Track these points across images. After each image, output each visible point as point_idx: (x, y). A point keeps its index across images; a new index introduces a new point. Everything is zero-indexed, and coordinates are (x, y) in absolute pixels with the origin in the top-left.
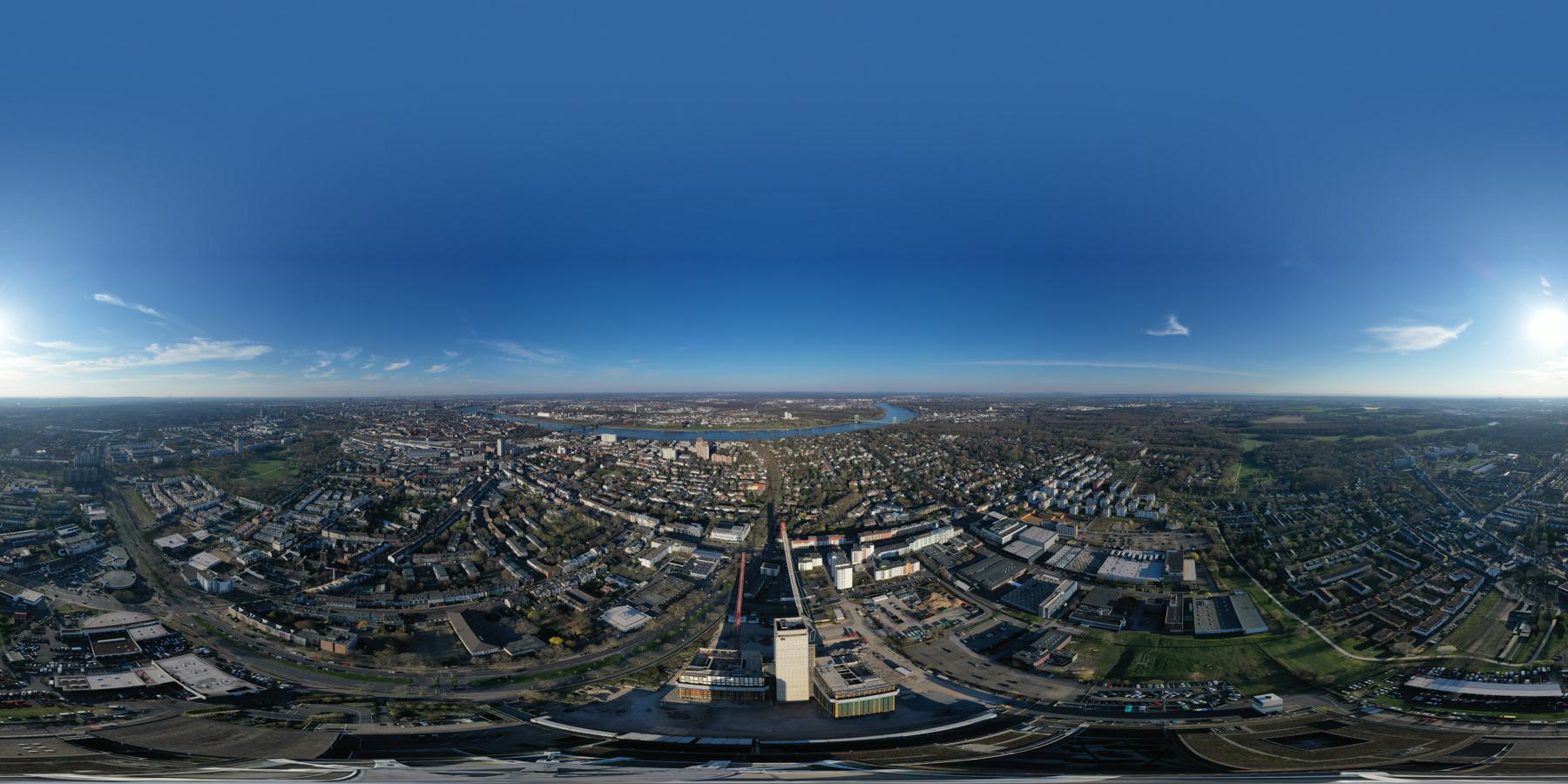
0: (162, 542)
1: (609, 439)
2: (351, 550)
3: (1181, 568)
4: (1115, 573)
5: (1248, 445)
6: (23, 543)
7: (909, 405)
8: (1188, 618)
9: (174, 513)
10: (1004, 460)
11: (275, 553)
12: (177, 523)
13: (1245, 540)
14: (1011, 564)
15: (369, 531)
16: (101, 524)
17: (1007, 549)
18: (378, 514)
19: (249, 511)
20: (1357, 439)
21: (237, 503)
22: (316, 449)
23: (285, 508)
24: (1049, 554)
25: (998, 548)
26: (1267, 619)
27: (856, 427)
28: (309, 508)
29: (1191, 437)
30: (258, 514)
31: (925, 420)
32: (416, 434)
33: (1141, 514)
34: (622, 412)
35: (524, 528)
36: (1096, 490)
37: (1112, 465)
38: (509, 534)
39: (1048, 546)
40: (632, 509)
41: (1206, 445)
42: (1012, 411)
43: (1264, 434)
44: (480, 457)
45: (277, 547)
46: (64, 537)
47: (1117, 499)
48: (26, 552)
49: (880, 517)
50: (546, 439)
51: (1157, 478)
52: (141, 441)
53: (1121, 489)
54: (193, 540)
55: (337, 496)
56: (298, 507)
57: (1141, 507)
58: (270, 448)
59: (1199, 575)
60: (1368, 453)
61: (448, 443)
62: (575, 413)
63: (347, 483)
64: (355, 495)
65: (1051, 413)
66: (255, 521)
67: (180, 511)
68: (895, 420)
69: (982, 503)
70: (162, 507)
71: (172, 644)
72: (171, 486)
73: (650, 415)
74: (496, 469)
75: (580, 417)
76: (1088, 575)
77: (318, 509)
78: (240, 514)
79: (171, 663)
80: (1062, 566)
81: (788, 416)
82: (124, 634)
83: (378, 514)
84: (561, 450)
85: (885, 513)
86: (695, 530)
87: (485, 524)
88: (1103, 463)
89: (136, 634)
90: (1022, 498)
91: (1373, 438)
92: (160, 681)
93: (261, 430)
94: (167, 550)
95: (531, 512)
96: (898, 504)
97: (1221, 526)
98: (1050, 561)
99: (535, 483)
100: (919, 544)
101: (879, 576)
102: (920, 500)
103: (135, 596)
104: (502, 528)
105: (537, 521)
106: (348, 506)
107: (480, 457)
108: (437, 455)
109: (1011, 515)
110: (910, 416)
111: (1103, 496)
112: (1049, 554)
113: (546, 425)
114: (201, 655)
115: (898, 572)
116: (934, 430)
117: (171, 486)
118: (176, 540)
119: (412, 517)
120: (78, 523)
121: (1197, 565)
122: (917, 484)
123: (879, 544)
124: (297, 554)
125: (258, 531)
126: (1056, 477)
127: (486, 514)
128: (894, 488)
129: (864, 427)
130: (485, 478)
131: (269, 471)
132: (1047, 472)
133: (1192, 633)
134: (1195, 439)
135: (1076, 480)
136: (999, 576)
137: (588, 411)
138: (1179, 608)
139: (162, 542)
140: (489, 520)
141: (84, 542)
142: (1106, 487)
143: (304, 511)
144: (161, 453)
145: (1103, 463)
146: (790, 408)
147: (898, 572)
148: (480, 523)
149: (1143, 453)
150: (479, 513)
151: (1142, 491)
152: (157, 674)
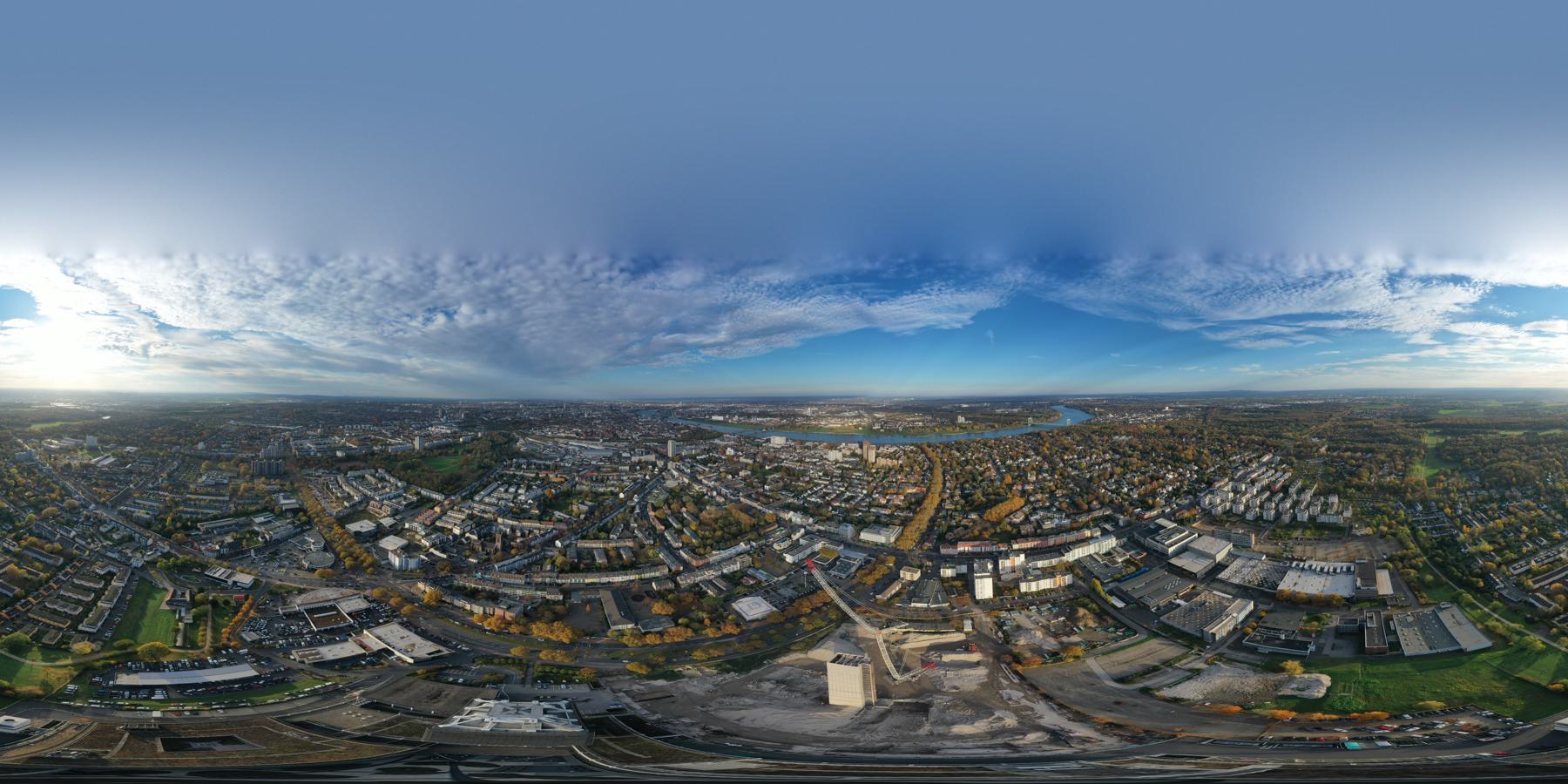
0: (354, 527)
1: (778, 441)
2: (523, 535)
3: (1374, 581)
4: (1297, 589)
5: (1430, 440)
6: (224, 531)
7: (1083, 405)
8: (1392, 638)
9: (360, 503)
10: (1176, 460)
11: (455, 536)
12: (364, 511)
13: (1442, 544)
14: (1177, 580)
15: (540, 519)
16: (295, 511)
17: (1174, 561)
18: (561, 500)
19: (430, 500)
20: (1541, 434)
21: (418, 494)
22: (493, 448)
23: (464, 499)
24: (1221, 567)
25: (1162, 557)
26: (1488, 632)
27: (1030, 430)
28: (487, 500)
29: (1372, 435)
30: (439, 503)
31: (1101, 420)
32: (590, 437)
33: (1323, 519)
34: (795, 415)
35: (682, 521)
36: (1273, 494)
37: (1291, 464)
38: (668, 526)
39: (1220, 557)
40: (788, 507)
41: (1388, 441)
42: (1189, 410)
43: (1445, 428)
44: (652, 458)
45: (457, 531)
46: (261, 524)
47: (1295, 504)
48: (229, 539)
49: (1039, 524)
50: (717, 441)
51: (1338, 480)
52: (322, 437)
53: (1301, 491)
54: (379, 525)
55: (512, 490)
56: (477, 498)
57: (1323, 512)
58: (448, 446)
59: (1395, 586)
60: (1553, 446)
61: (621, 445)
62: (749, 416)
63: (522, 478)
64: (529, 488)
65: (1228, 411)
66: (437, 509)
67: (366, 499)
68: (1069, 422)
69: (1151, 508)
70: (349, 497)
71: (368, 618)
72: (356, 478)
73: (823, 417)
74: (665, 469)
75: (753, 420)
76: (1264, 594)
77: (494, 501)
78: (424, 502)
79: (380, 631)
80: (1236, 581)
81: (961, 419)
82: (334, 608)
83: (547, 507)
84: (730, 452)
85: (1042, 520)
86: (848, 531)
87: (646, 517)
88: (1282, 462)
89: (346, 607)
90: (1195, 503)
91: (1558, 431)
92: (376, 648)
93: (440, 430)
94: (357, 534)
95: (692, 507)
96: (1059, 510)
97: (1413, 530)
98: (1222, 575)
99: (700, 482)
100: (1073, 556)
101: (1024, 587)
102: (1079, 503)
103: (338, 575)
104: (664, 522)
105: (696, 517)
106: (522, 498)
107: (652, 458)
108: (610, 454)
109: (1181, 522)
110: (1084, 417)
111: (1283, 500)
112: (1221, 567)
113: (720, 429)
114: (401, 624)
115: (1046, 584)
116: (1106, 431)
117: (356, 478)
118: (365, 526)
119: (579, 508)
120: (272, 511)
121: (1392, 575)
122: (1087, 487)
123: (1030, 554)
124: (475, 537)
125: (439, 518)
126: (1232, 479)
127: (649, 508)
128: (1059, 493)
129: (1036, 430)
130: (653, 476)
131: (450, 464)
132: (1222, 472)
133: (1402, 657)
134: (1376, 435)
135: (1253, 482)
136: (1161, 592)
137: (763, 414)
138: (1380, 628)
139: (354, 527)
140: (652, 514)
141: (282, 527)
142: (1285, 489)
143: (481, 501)
144: (343, 448)
145: (1282, 462)
146: (964, 412)
147: (1046, 584)
148: (644, 515)
149: (1323, 450)
150: (644, 509)
151: (1324, 493)
152: (371, 640)
